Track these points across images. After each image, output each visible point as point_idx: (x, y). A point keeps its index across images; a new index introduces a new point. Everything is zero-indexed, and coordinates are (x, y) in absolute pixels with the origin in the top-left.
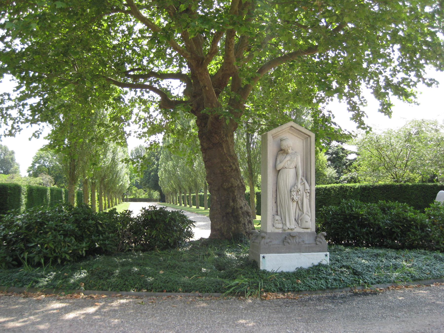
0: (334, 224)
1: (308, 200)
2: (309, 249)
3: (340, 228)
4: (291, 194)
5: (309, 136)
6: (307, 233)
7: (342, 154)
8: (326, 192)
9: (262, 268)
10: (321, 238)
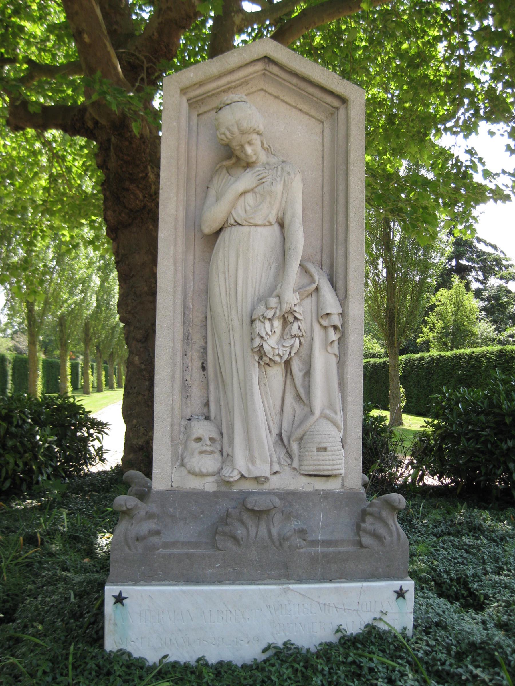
0: (468, 440)
1: (334, 361)
2: (328, 567)
3: (482, 452)
4: (252, 331)
5: (344, 100)
6: (327, 495)
7: (506, 300)
8: (472, 362)
9: (110, 644)
10: (379, 518)
